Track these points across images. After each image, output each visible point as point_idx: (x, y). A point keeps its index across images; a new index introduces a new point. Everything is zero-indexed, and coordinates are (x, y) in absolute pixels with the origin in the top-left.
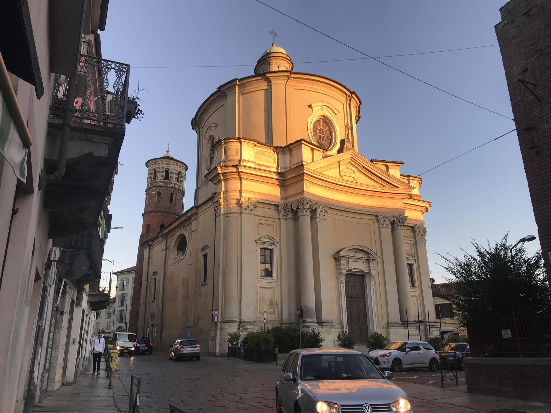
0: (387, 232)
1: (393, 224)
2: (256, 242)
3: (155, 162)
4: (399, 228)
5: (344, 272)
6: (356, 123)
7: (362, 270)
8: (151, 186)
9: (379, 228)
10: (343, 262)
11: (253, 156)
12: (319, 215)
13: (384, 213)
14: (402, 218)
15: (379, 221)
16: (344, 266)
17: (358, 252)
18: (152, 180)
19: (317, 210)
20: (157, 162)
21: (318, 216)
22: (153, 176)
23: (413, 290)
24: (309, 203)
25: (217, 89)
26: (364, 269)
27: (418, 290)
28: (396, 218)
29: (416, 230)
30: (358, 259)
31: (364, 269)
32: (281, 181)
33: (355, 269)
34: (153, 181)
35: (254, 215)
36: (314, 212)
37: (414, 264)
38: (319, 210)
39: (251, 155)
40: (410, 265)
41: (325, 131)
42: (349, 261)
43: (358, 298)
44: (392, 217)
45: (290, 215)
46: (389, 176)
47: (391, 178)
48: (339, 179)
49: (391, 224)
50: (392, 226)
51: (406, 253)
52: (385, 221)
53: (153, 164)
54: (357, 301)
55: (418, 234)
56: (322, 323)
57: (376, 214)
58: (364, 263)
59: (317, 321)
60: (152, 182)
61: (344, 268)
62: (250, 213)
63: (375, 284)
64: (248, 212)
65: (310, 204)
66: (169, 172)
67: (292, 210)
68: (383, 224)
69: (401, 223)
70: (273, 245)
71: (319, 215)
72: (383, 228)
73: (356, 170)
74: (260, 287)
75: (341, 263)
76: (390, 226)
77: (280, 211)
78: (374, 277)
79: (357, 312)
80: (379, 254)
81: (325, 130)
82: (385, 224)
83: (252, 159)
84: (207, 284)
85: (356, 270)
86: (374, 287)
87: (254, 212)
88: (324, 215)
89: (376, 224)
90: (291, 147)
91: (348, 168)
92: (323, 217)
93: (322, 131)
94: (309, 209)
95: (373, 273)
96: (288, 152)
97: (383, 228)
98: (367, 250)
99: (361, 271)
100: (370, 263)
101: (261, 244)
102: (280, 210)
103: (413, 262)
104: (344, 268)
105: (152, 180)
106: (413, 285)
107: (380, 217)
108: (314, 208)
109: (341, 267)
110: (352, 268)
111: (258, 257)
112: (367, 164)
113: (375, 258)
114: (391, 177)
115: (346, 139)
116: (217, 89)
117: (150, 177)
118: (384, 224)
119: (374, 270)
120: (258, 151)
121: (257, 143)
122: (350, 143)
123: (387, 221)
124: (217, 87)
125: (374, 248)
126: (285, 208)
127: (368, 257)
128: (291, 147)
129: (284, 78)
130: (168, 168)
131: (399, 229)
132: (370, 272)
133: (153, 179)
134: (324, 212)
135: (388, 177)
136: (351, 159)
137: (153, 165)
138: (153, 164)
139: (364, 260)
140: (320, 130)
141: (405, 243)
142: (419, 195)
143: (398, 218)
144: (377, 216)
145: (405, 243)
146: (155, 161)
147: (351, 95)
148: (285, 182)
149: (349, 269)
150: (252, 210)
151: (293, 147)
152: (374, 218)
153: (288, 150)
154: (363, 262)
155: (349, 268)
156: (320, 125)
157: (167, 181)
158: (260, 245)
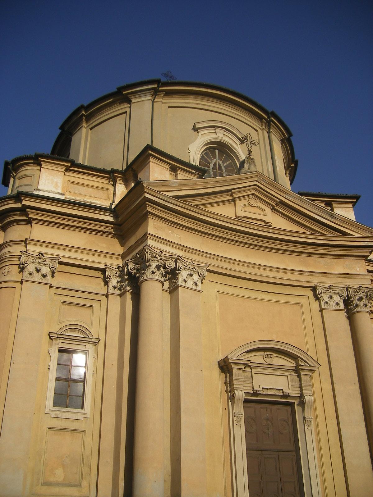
1: (347, 302)
2: (50, 338)
4: (362, 310)
5: (239, 394)
6: (291, 183)
7: (283, 392)
9: (321, 311)
10: (238, 374)
11: (60, 184)
13: (328, 283)
14: (366, 291)
15: (319, 296)
16: (240, 383)
17: (275, 355)
19: (178, 272)
24: (159, 258)
28: (355, 292)
30: (274, 369)
33: (267, 389)
35: (51, 286)
36: (172, 274)
38: (184, 274)
39: (57, 183)
41: (225, 167)
42: (253, 373)
43: (278, 451)
44: (345, 289)
46: (332, 216)
47: (336, 219)
49: (345, 301)
52: (331, 297)
57: (313, 285)
58: (289, 376)
61: (242, 387)
62: (40, 281)
64: (36, 280)
68: (327, 303)
69: (364, 300)
70: (87, 345)
71: (185, 281)
72: (328, 309)
73: (268, 210)
76: (342, 306)
80: (323, 359)
81: (225, 164)
82: (332, 305)
83: (60, 191)
85: (269, 392)
86: (313, 426)
87: (49, 280)
88: (196, 284)
89: (315, 305)
90: (134, 167)
91: (252, 206)
92: (194, 287)
93: (220, 166)
97: (328, 309)
98: (293, 350)
99: (281, 394)
100: (33, 224)
101: (61, 341)
104: (242, 387)
107: (319, 290)
108: (173, 265)
112: (287, 197)
113: (310, 366)
114: (337, 217)
115: (246, 159)
118: (331, 304)
123: (337, 298)
127: (298, 365)
128: (134, 167)
129: (150, 92)
131: (360, 312)
132: (302, 396)
134: (196, 277)
135: (330, 218)
136: (256, 190)
139: (287, 370)
140: (215, 164)
143: (357, 292)
149: (253, 390)
150: (44, 276)
152: (310, 294)
154: (287, 376)
156: (215, 158)
158: (58, 344)
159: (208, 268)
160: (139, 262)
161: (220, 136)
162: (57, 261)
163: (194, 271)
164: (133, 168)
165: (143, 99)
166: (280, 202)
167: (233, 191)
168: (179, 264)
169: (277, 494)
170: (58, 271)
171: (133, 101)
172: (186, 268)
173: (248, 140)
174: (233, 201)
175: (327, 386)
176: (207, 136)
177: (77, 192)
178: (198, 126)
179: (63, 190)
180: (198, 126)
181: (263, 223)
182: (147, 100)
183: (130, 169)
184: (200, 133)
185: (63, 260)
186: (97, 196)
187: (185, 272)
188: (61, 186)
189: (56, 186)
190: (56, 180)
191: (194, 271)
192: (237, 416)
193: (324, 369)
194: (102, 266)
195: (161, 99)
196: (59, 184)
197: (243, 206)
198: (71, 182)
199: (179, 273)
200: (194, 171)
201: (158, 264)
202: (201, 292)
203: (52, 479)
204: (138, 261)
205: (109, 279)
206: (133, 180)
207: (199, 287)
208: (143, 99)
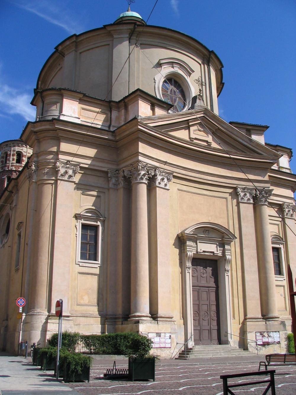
0: (247, 210)
1: (255, 198)
3: (7, 145)
6: (218, 96)
8: (2, 170)
12: (160, 183)
14: (267, 192)
18: (3, 164)
20: (9, 145)
21: (157, 184)
22: (4, 160)
23: (279, 278)
25: (54, 49)
26: (217, 251)
27: (285, 278)
29: (284, 208)
31: (217, 251)
32: (114, 142)
34: (4, 165)
36: (152, 180)
37: (282, 249)
38: (159, 178)
39: (74, 109)
40: (276, 250)
45: (122, 184)
48: (189, 142)
50: (254, 200)
51: (271, 236)
53: (4, 147)
54: (208, 290)
55: (287, 214)
56: (157, 317)
59: (151, 316)
60: (3, 167)
63: (232, 270)
65: (146, 169)
66: (21, 155)
67: (124, 177)
74: (80, 273)
75: (187, 244)
76: (252, 201)
77: (109, 179)
78: (230, 261)
79: (208, 305)
80: (237, 235)
82: (246, 199)
84: (19, 268)
86: (229, 274)
90: (126, 100)
94: (144, 175)
95: (228, 257)
96: (124, 108)
102: (110, 178)
103: (281, 246)
105: (3, 164)
106: (279, 272)
108: (153, 174)
109: (187, 248)
110: (201, 250)
111: (77, 236)
115: (198, 96)
116: (54, 49)
117: (2, 161)
118: (245, 198)
119: (230, 254)
120: (201, 89)
121: (84, 96)
122: (203, 101)
124: (55, 47)
125: (233, 228)
126: (117, 175)
130: (20, 150)
133: (4, 163)
134: (166, 180)
137: (5, 148)
138: (4, 147)
141: (270, 224)
142: (290, 168)
144: (235, 189)
145: (270, 224)
146: (7, 143)
147: (210, 55)
148: (118, 143)
151: (128, 101)
153: (123, 105)
155: (197, 250)
157: (18, 164)
159: (80, 166)
160: (132, 170)
161: (177, 70)
162: (79, 167)
163: (165, 176)
164: (125, 101)
165: (122, 36)
166: (218, 129)
167: (190, 121)
168: (157, 172)
169: (198, 312)
170: (173, 182)
171: (115, 36)
172: (160, 175)
173: (199, 81)
174: (188, 128)
175: (238, 250)
176: (166, 70)
177: (87, 116)
178: (161, 62)
179: (78, 116)
180: (162, 62)
181: (205, 144)
182: (125, 37)
183: (123, 101)
184: (163, 67)
185: (175, 174)
186: (100, 119)
187: (160, 177)
188: (77, 112)
189: (74, 112)
190: (73, 107)
191: (165, 176)
192: (188, 267)
193: (237, 241)
194: (105, 170)
195: (135, 37)
196: (76, 110)
197: (195, 131)
198: (83, 109)
199: (157, 178)
200: (165, 106)
201: (145, 172)
202: (168, 190)
203: (82, 302)
204: (131, 169)
205: (110, 179)
206: (124, 109)
207: (167, 188)
208: (122, 36)
